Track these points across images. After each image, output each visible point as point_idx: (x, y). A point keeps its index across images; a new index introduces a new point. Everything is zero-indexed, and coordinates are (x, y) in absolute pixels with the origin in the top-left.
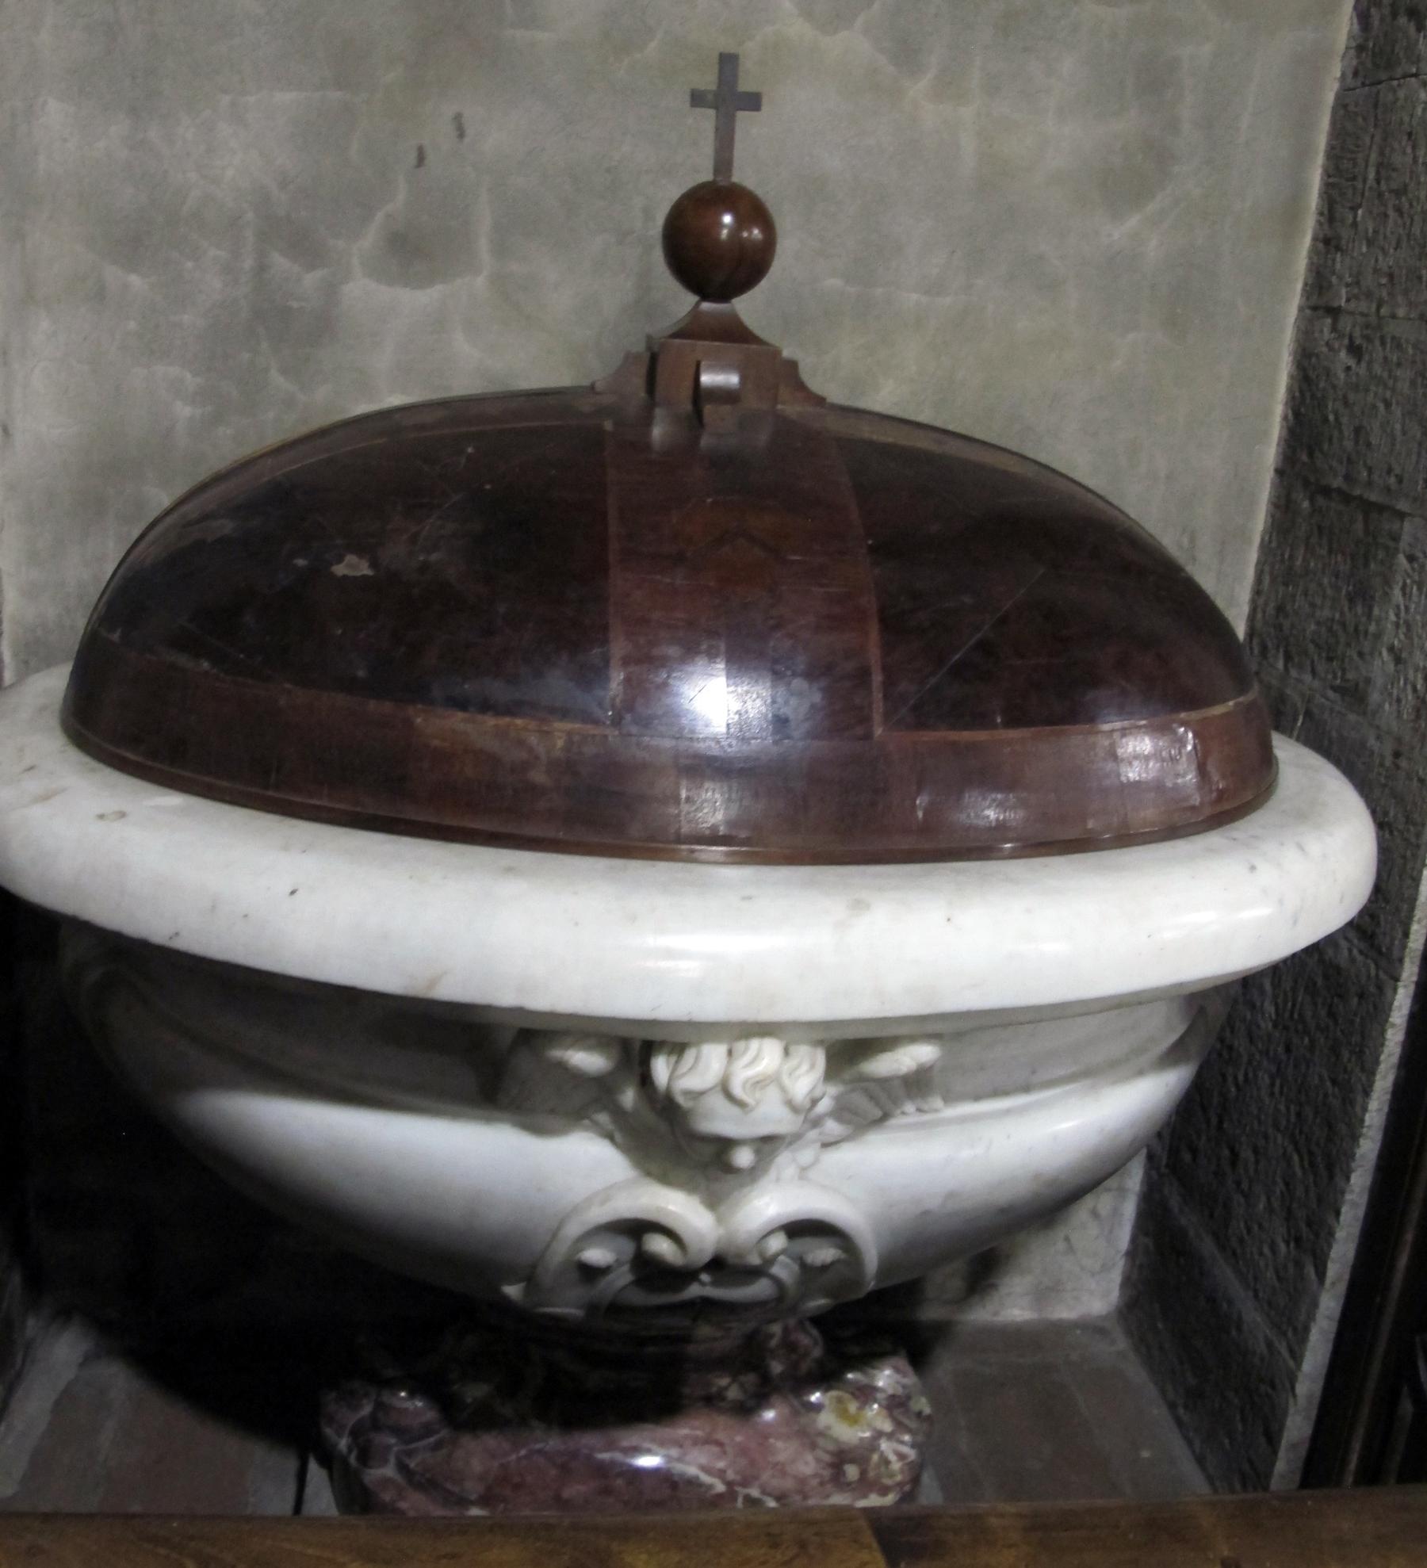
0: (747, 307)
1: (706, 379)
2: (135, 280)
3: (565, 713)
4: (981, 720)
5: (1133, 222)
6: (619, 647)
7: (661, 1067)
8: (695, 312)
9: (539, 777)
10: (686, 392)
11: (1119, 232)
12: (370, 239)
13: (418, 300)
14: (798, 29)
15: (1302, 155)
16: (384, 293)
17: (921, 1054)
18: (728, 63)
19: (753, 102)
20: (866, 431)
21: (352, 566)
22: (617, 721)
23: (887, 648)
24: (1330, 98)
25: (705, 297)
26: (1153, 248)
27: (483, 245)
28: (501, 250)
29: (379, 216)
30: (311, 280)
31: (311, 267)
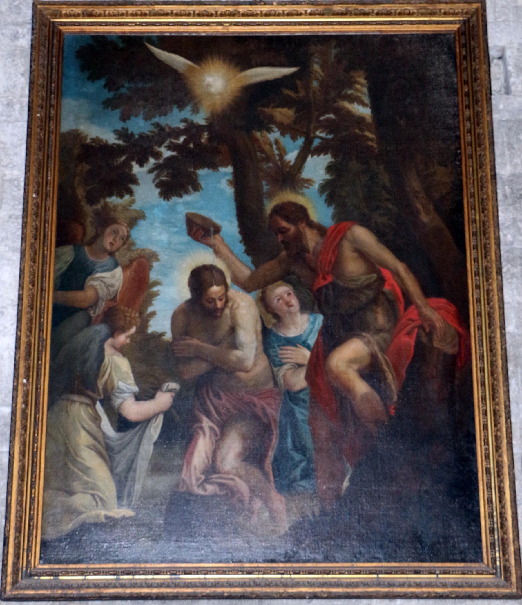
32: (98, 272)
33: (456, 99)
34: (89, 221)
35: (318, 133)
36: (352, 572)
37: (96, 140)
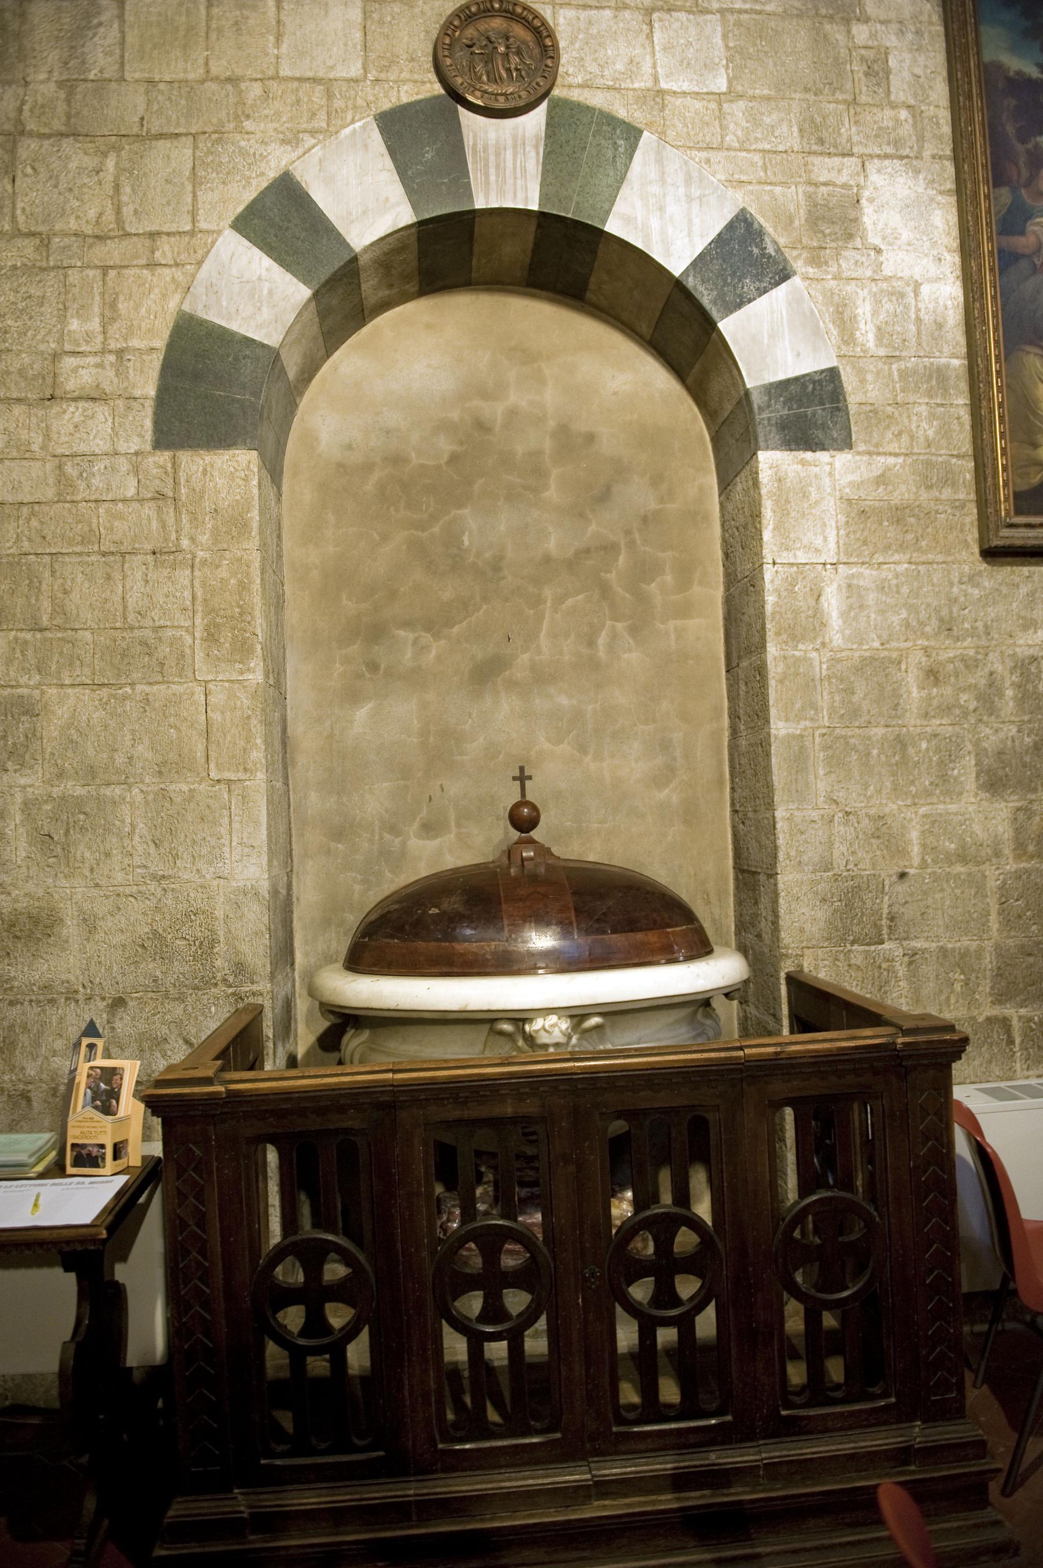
0: (535, 834)
1: (524, 854)
2: (339, 845)
3: (494, 940)
4: (604, 932)
5: (667, 791)
6: (506, 922)
7: (527, 1028)
8: (520, 838)
9: (489, 957)
10: (519, 858)
11: (663, 795)
12: (415, 826)
13: (432, 844)
14: (547, 746)
15: (720, 762)
16: (421, 842)
17: (595, 1020)
18: (522, 769)
19: (530, 778)
20: (572, 865)
21: (434, 911)
22: (507, 941)
23: (577, 916)
24: (726, 743)
25: (522, 832)
26: (675, 799)
27: (453, 824)
28: (459, 826)
29: (418, 819)
30: (398, 841)
31: (397, 836)
32: (1037, 217)
33: (929, 988)
34: (1022, 161)
35: (507, 1246)
36: (370, 287)
37: (1019, 73)
